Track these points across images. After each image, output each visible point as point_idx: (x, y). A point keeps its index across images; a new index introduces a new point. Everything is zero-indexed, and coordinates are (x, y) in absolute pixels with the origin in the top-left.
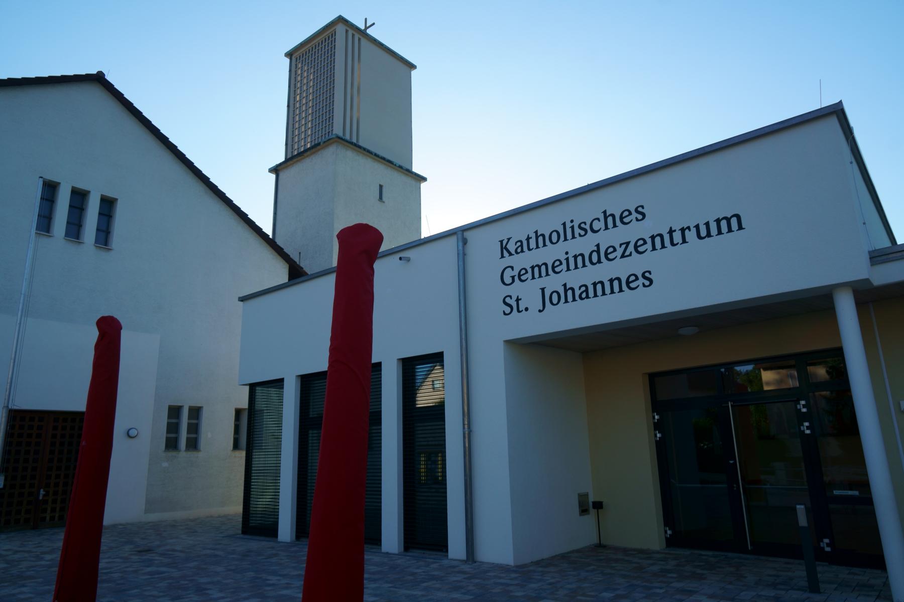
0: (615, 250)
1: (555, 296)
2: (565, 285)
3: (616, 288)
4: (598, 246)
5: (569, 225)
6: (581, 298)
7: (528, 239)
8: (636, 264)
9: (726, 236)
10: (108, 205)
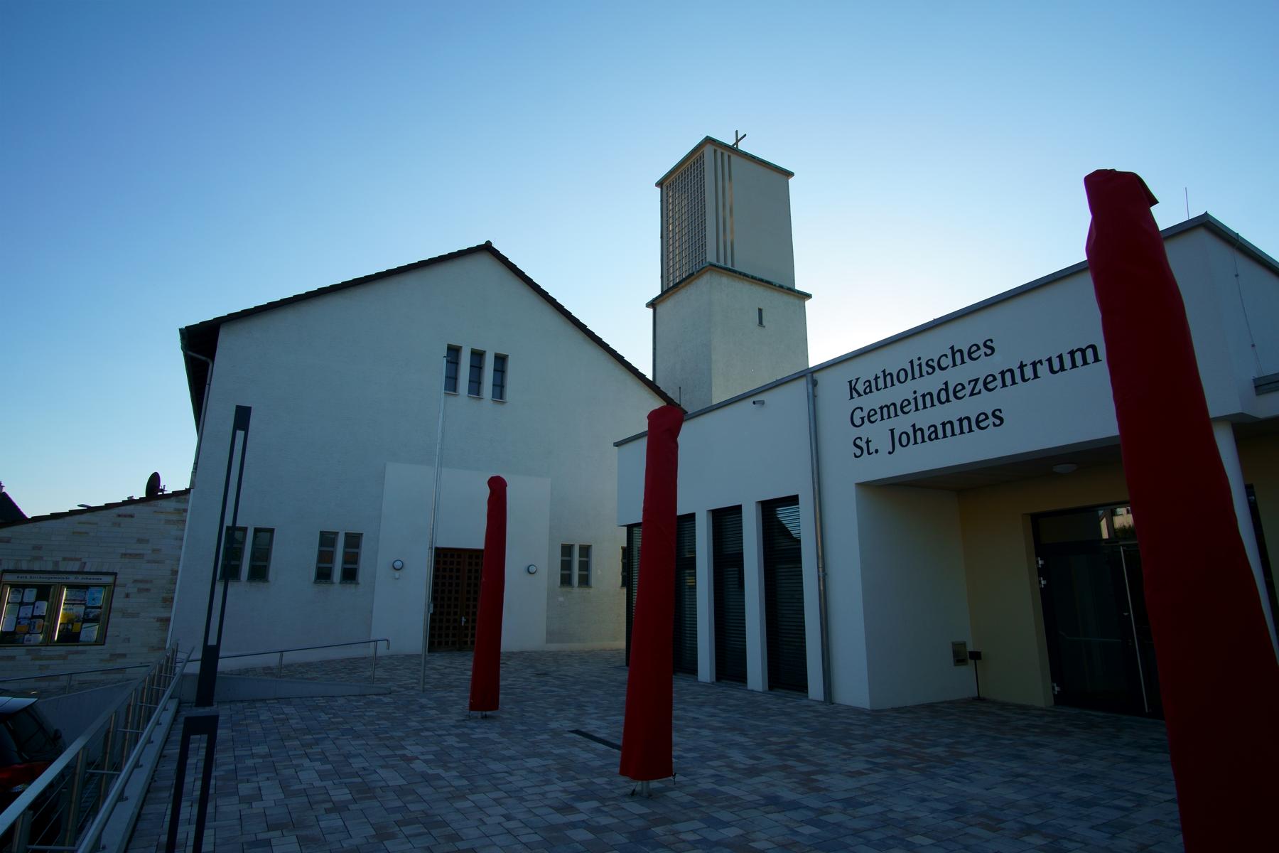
0: (964, 388)
1: (904, 438)
2: (914, 426)
3: (966, 428)
4: (946, 384)
5: (916, 363)
6: (930, 439)
7: (876, 378)
8: (985, 403)
9: (1081, 370)
10: (501, 360)
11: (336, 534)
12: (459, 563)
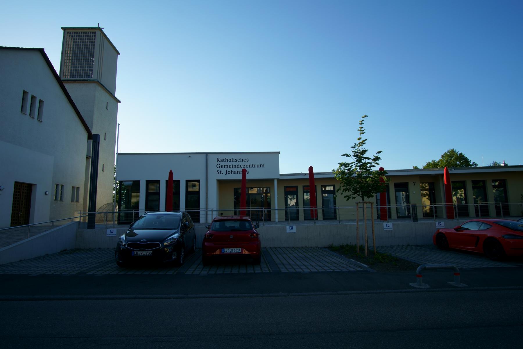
10: (41, 102)
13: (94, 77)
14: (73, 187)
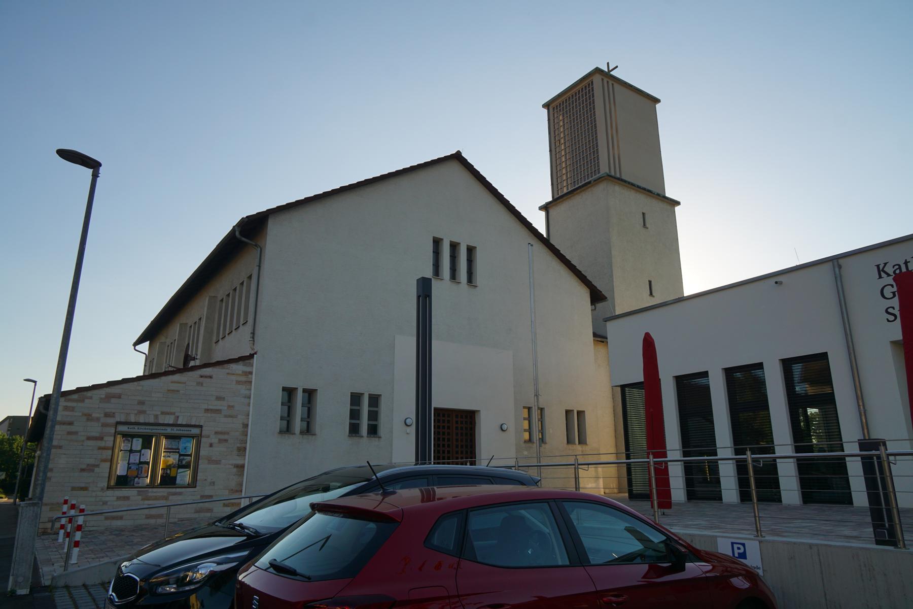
10: (471, 250)
11: (362, 394)
12: (449, 421)
13: (604, 169)
14: (568, 413)
